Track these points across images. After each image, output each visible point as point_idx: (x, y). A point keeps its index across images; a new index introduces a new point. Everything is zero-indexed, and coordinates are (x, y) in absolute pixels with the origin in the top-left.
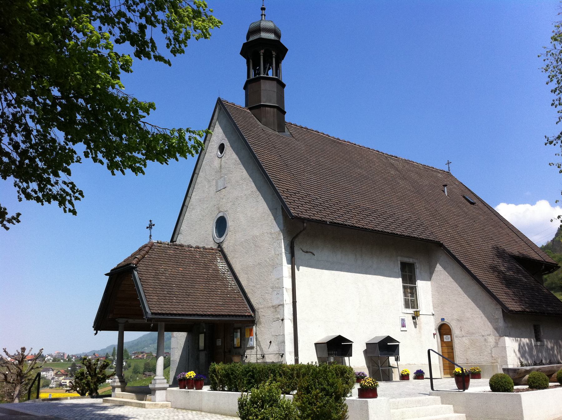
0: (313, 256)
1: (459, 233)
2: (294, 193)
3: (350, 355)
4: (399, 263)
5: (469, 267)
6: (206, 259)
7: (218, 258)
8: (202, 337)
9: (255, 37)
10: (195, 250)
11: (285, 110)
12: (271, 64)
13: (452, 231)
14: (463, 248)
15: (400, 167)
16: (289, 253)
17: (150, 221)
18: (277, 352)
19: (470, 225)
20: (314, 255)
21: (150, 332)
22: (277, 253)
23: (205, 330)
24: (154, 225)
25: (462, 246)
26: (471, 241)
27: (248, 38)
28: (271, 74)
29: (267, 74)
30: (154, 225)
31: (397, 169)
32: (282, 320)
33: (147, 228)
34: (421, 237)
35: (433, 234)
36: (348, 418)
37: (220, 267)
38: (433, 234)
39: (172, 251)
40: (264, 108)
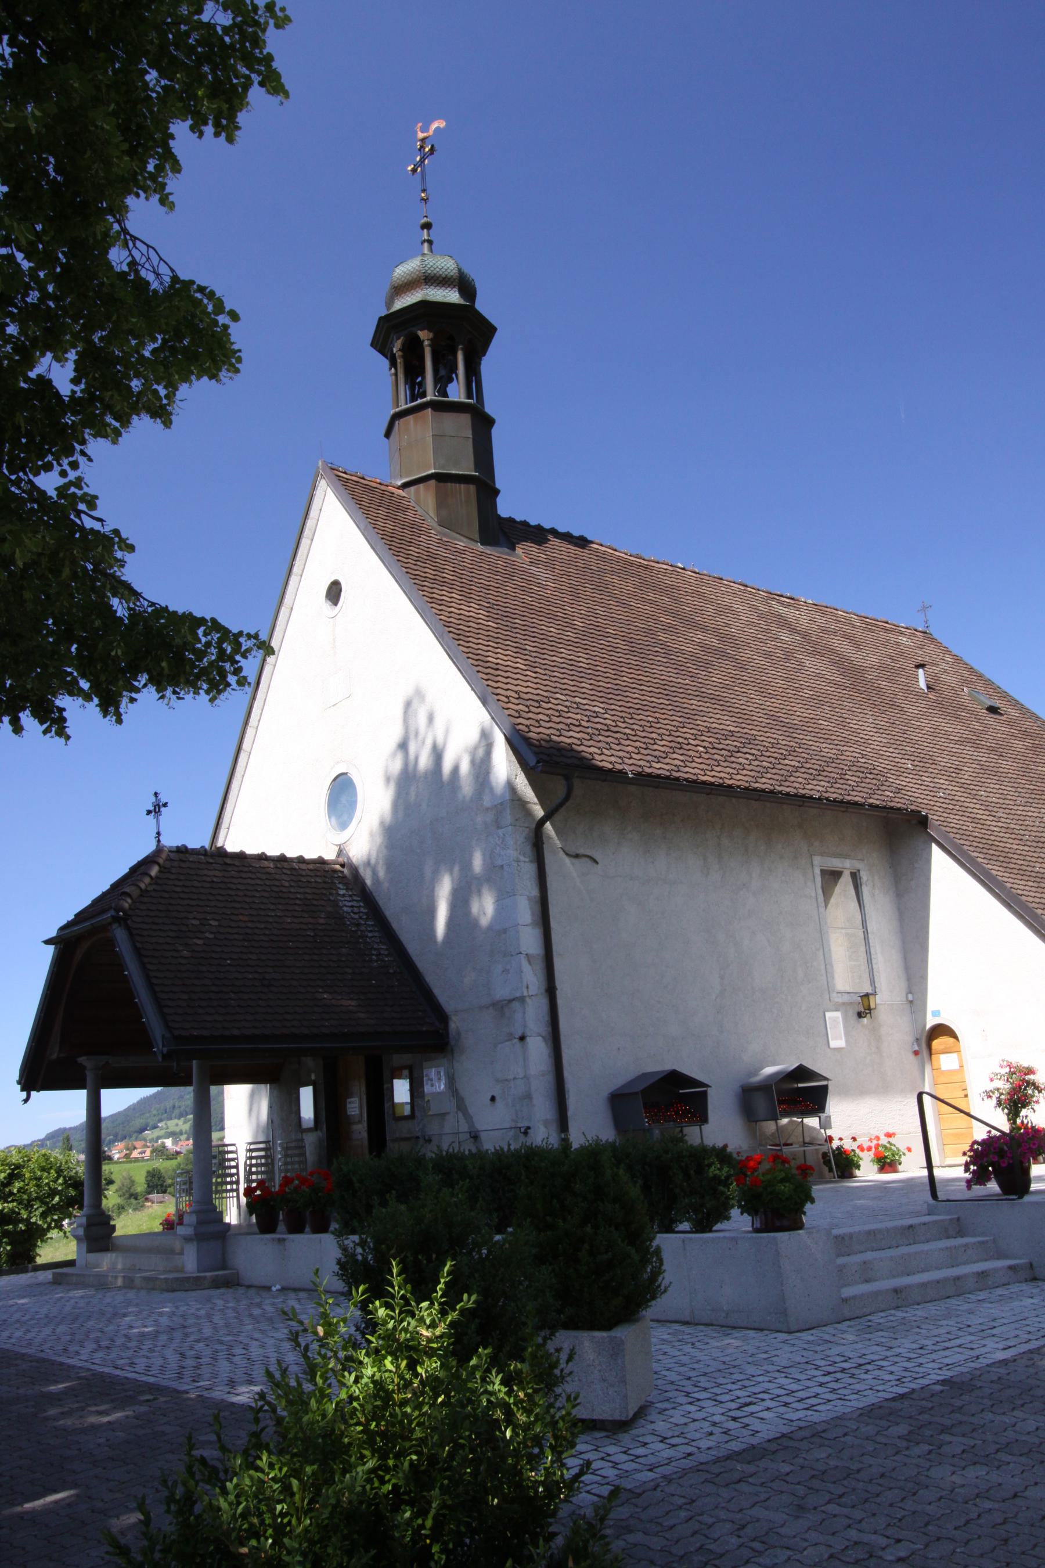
0: (595, 865)
1: (966, 786)
2: (537, 701)
3: (704, 1119)
4: (817, 871)
5: (999, 873)
6: (308, 890)
7: (341, 886)
8: (306, 1095)
9: (409, 299)
10: (279, 866)
11: (498, 485)
12: (454, 369)
13: (947, 783)
14: (980, 826)
15: (804, 621)
16: (531, 861)
17: (156, 794)
18: (513, 1125)
19: (992, 764)
20: (596, 862)
21: (159, 1089)
22: (499, 862)
23: (313, 1077)
24: (165, 805)
25: (977, 821)
26: (998, 805)
27: (390, 302)
28: (456, 392)
29: (446, 395)
30: (165, 805)
31: (793, 630)
32: (522, 1038)
33: (149, 812)
34: (871, 801)
35: (903, 792)
36: (665, 1291)
37: (345, 909)
38: (903, 792)
39: (217, 873)
40: (458, 485)
